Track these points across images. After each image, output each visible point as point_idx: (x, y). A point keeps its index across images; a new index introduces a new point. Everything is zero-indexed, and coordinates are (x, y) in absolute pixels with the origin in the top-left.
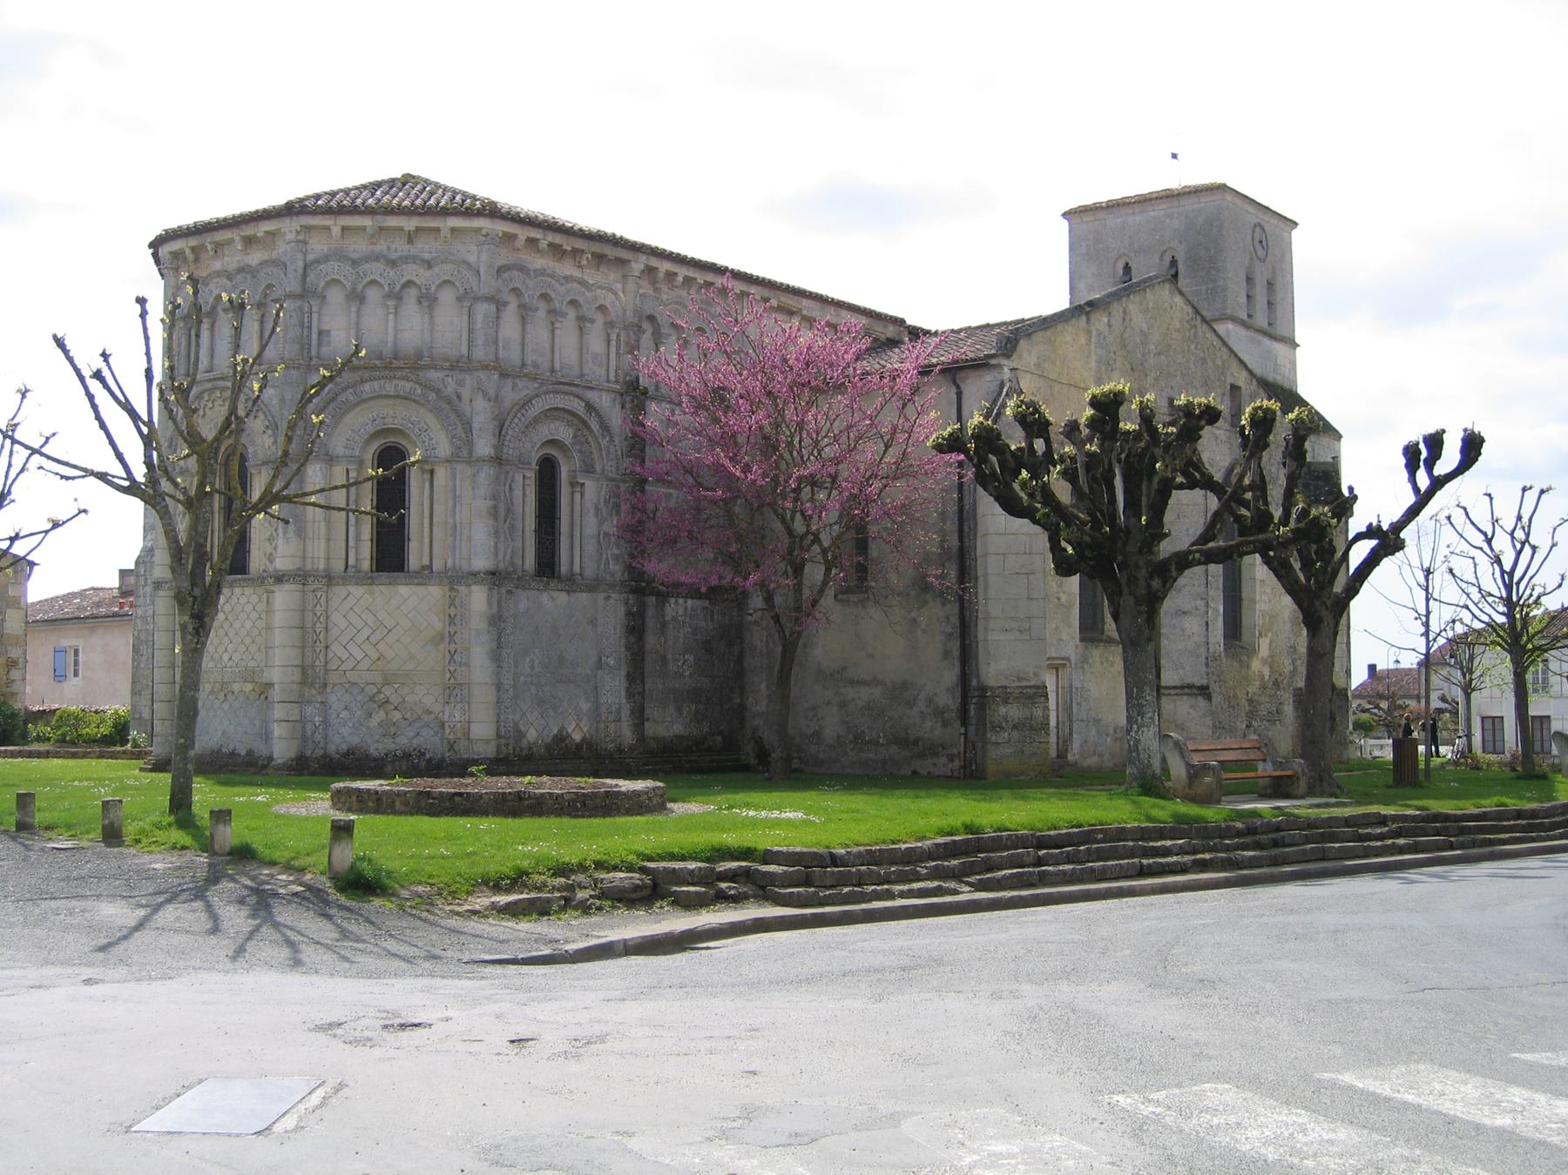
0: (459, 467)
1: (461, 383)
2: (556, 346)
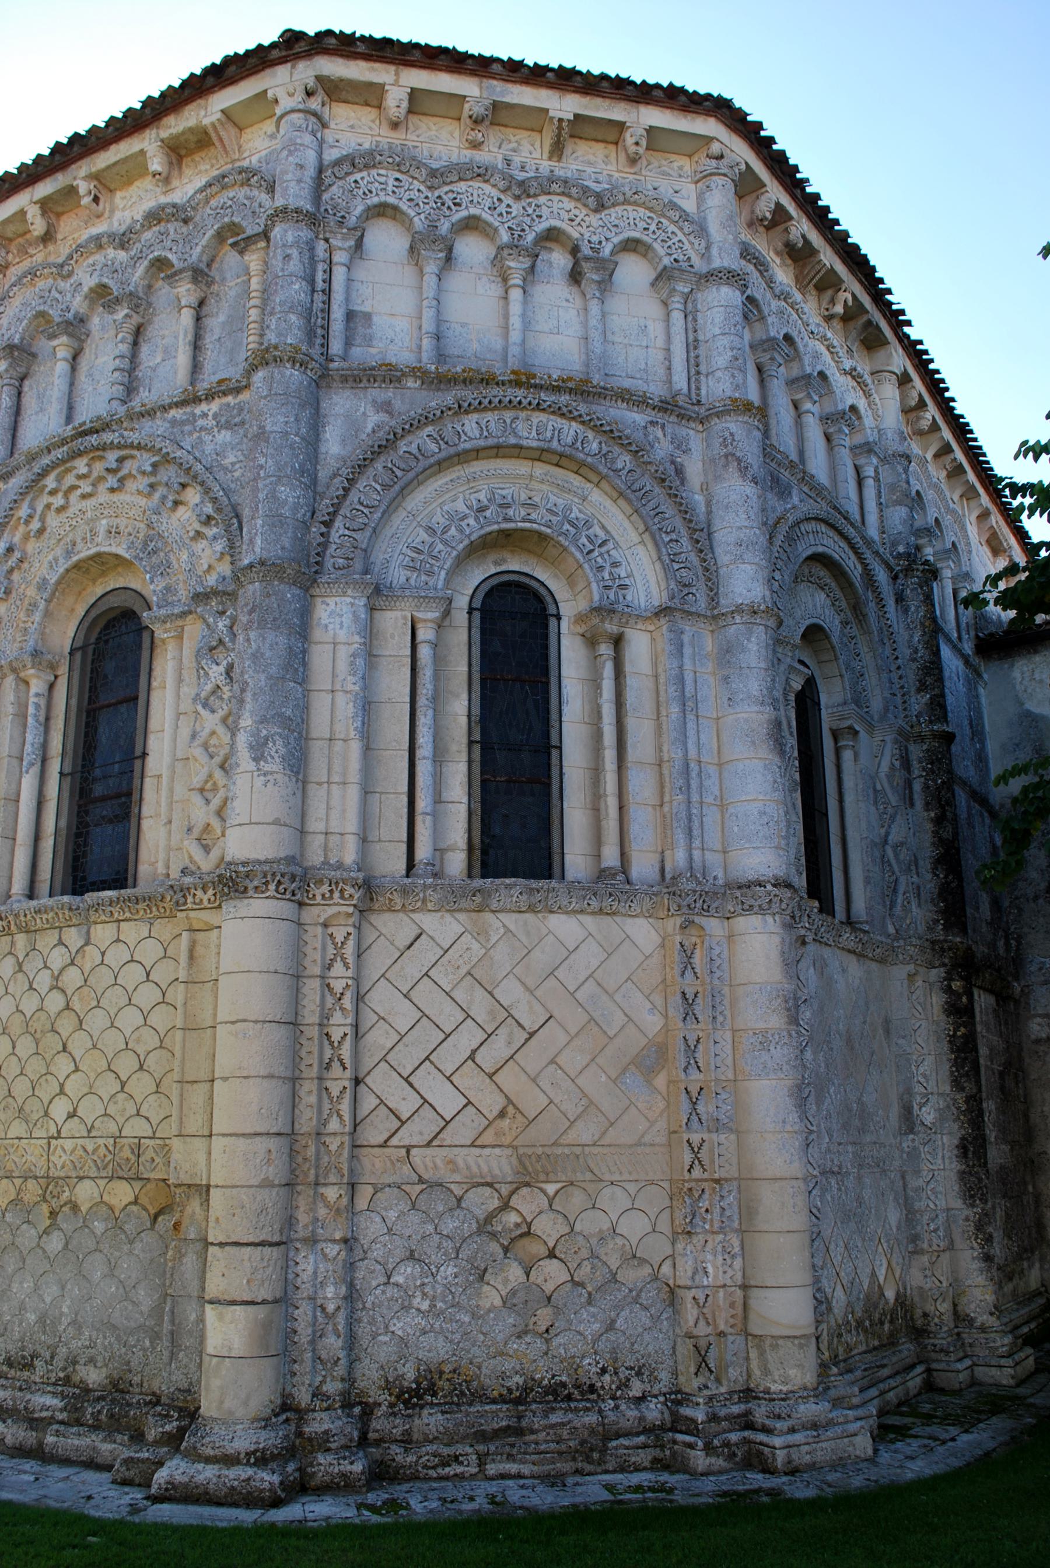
0: (689, 628)
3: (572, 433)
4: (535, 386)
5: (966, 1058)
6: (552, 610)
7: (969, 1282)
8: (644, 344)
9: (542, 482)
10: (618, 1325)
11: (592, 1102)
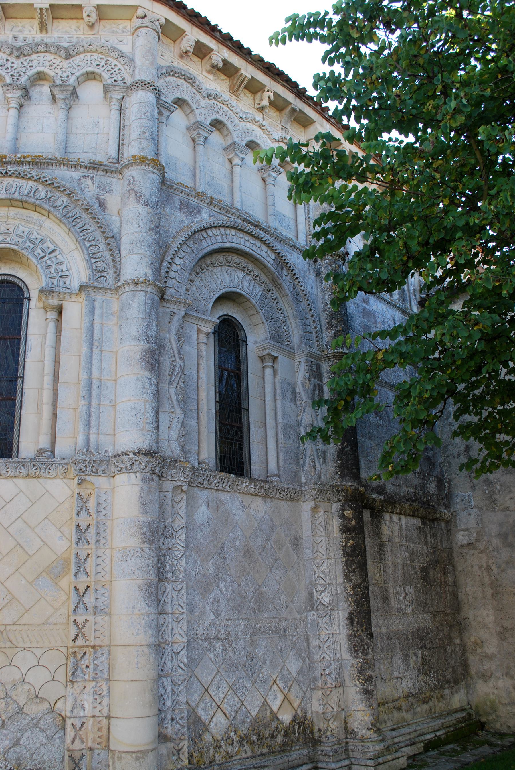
0: (99, 298)
1: (106, 189)
2: (236, 185)
3: (29, 187)
4: (6, 163)
5: (353, 560)
6: (26, 295)
7: (354, 708)
8: (96, 132)
9: (15, 219)
10: (22, 742)
11: (14, 597)
